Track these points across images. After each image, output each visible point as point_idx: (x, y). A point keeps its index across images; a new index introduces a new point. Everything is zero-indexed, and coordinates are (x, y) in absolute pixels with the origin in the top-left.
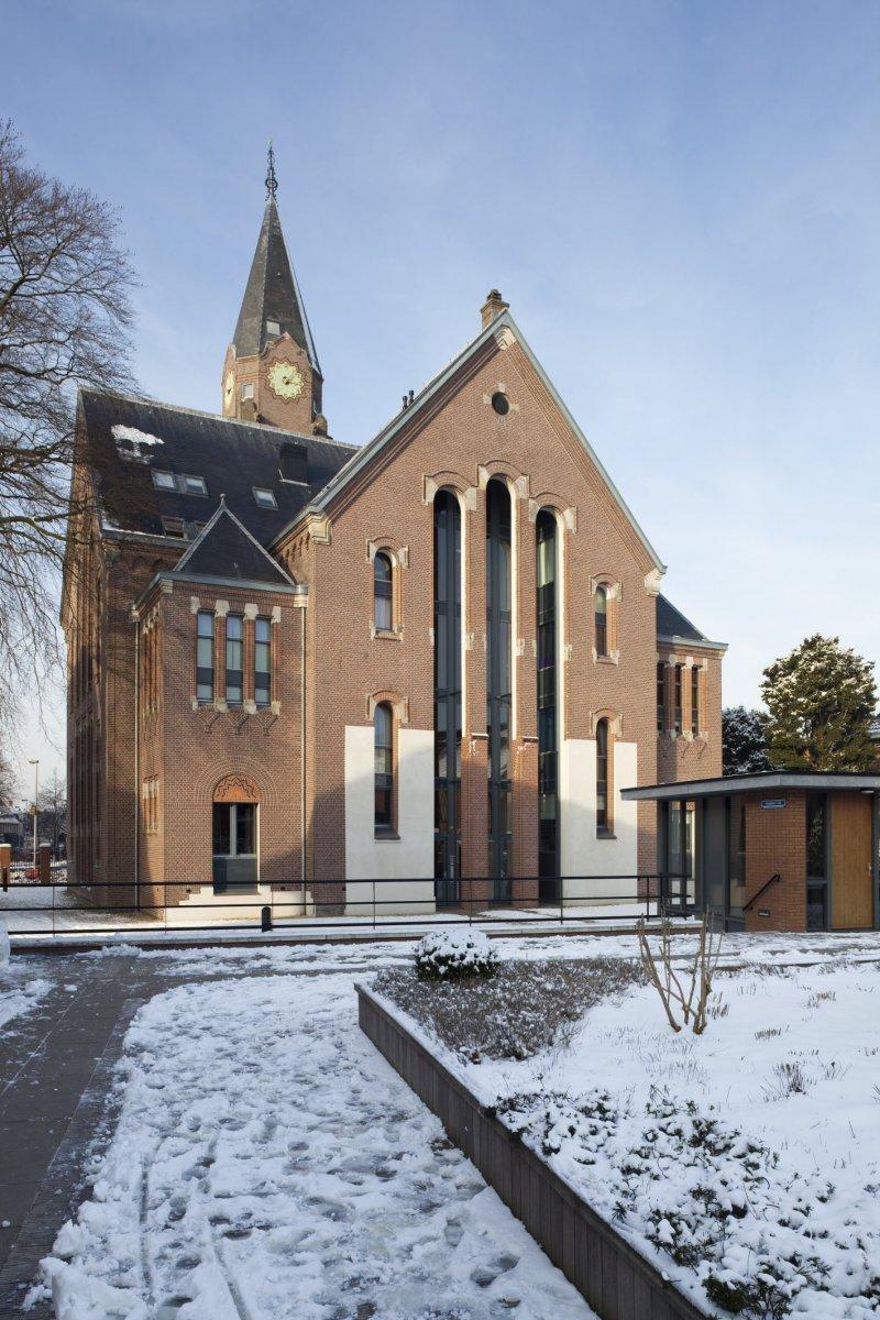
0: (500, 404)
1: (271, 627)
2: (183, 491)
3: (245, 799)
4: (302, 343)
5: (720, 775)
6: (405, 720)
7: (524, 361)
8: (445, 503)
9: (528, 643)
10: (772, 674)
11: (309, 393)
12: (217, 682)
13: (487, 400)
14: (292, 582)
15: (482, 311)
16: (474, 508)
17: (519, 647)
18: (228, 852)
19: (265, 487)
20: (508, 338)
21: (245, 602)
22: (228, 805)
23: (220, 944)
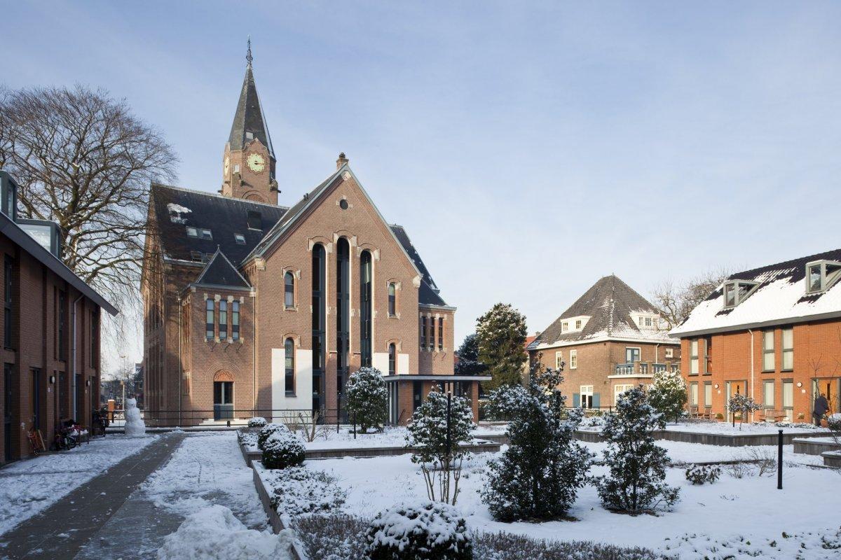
0: (343, 204)
1: (239, 305)
2: (201, 237)
3: (228, 380)
4: (265, 143)
5: (388, 375)
7: (355, 185)
8: (318, 249)
9: (356, 311)
10: (482, 320)
11: (268, 169)
12: (215, 330)
13: (338, 203)
14: (249, 285)
15: (337, 162)
16: (331, 252)
17: (353, 312)
18: (221, 403)
19: (241, 233)
20: (347, 176)
21: (227, 295)
23: (210, 430)
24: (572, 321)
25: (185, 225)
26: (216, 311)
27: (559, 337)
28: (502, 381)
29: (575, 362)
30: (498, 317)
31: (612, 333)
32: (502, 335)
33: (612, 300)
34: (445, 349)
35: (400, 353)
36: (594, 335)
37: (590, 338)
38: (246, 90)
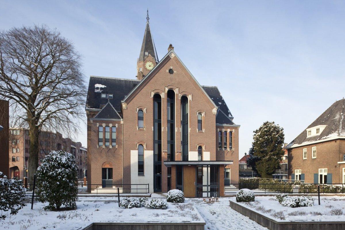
0: (171, 71)
3: (109, 167)
4: (154, 56)
6: (146, 148)
7: (177, 60)
8: (157, 97)
10: (256, 132)
13: (168, 71)
15: (168, 49)
18: (106, 179)
20: (173, 55)
22: (106, 168)
24: (314, 130)
25: (101, 93)
26: (105, 132)
27: (305, 139)
28: (267, 166)
29: (315, 154)
30: (265, 129)
31: (341, 134)
32: (268, 140)
33: (342, 114)
34: (233, 149)
35: (204, 151)
36: (328, 136)
37: (326, 138)
38: (146, 34)
